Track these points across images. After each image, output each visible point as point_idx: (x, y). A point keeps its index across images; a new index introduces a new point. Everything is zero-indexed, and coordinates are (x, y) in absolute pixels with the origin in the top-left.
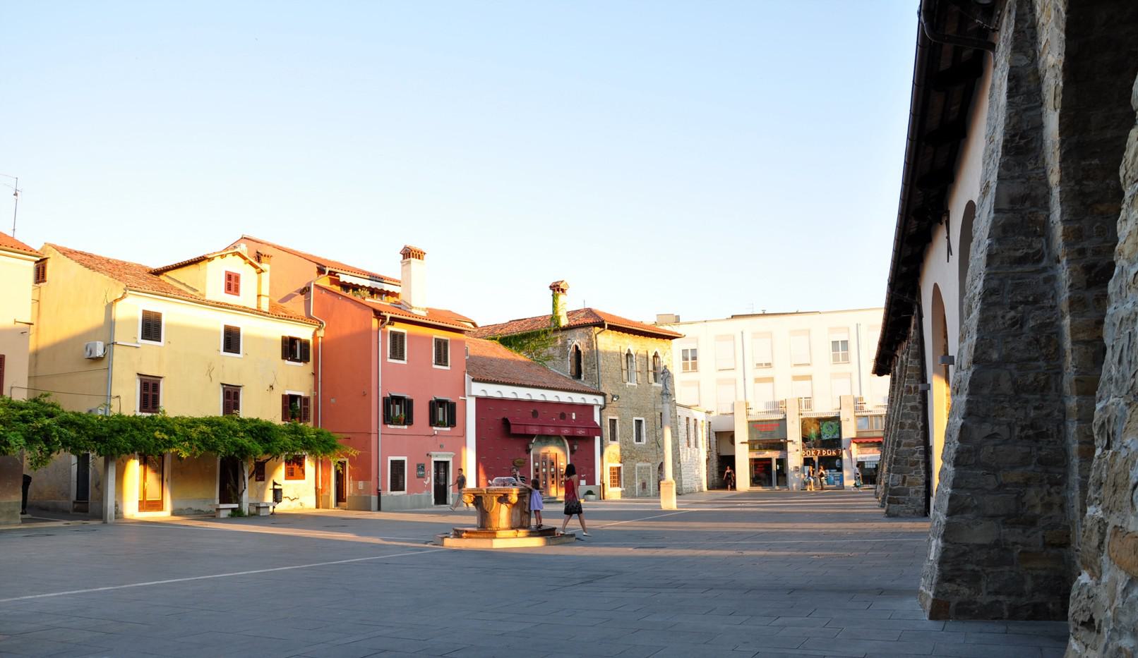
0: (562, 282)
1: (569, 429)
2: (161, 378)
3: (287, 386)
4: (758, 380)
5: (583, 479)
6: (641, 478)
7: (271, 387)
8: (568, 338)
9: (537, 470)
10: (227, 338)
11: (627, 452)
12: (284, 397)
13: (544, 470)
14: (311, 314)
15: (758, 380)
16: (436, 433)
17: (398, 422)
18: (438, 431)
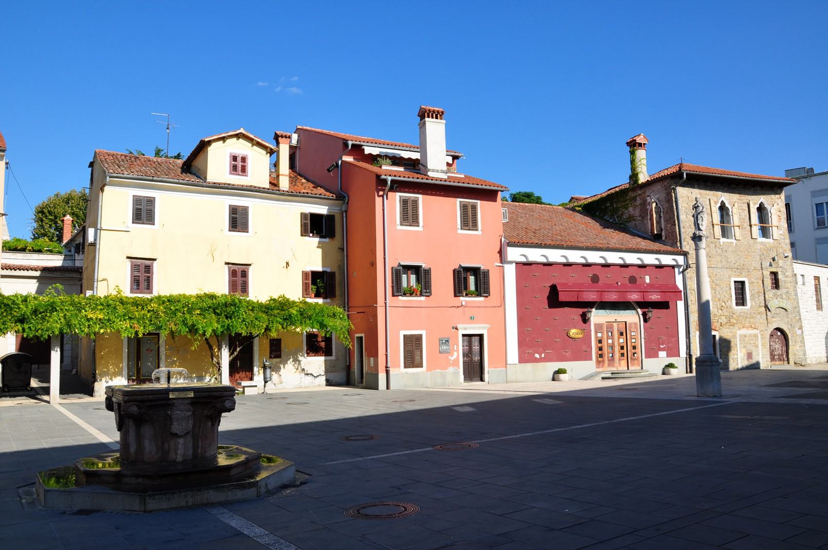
1: (617, 293)
2: (155, 260)
5: (663, 350)
6: (745, 347)
7: (287, 263)
8: (646, 195)
9: (600, 341)
10: (137, 209)
11: (723, 318)
13: (610, 341)
16: (464, 304)
17: (411, 293)
18: (466, 302)
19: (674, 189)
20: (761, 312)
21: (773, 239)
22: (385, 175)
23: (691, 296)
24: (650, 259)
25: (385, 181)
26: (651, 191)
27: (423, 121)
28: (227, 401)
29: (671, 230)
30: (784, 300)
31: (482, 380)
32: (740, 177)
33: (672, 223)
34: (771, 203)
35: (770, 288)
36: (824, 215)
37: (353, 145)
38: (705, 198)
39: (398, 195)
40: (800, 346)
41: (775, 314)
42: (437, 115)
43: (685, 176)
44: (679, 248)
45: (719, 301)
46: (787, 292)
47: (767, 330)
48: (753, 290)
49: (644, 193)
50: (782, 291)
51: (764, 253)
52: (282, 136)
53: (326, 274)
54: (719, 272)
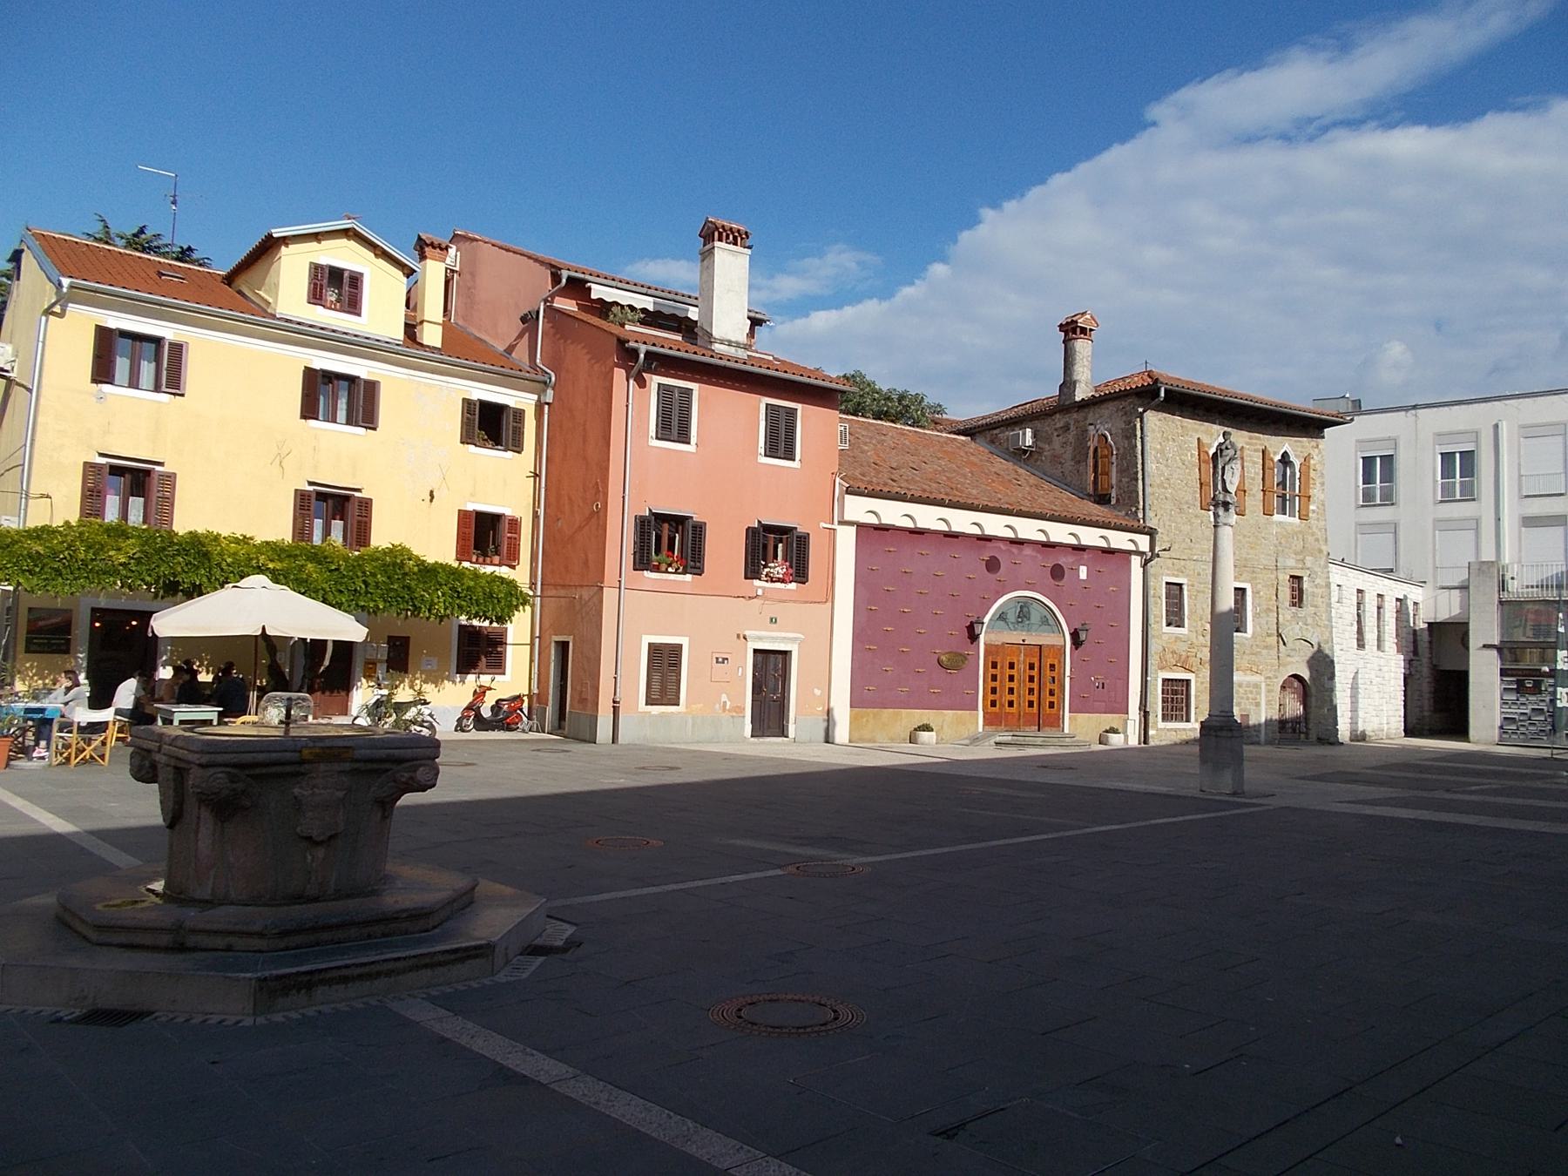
0: (1083, 314)
3: (472, 495)
4: (1529, 522)
12: (463, 516)
14: (538, 361)
15: (1529, 522)
16: (760, 592)
18: (764, 589)
19: (1141, 416)
20: (1271, 645)
21: (1300, 518)
22: (636, 341)
23: (1154, 609)
24: (1091, 537)
25: (634, 353)
26: (1097, 416)
27: (707, 247)
28: (421, 769)
29: (1128, 487)
30: (1309, 627)
31: (783, 732)
32: (1257, 404)
33: (1133, 476)
34: (1301, 454)
35: (1287, 604)
37: (569, 279)
38: (1191, 436)
39: (655, 381)
40: (1328, 710)
41: (1292, 650)
42: (736, 237)
43: (1162, 394)
44: (1142, 521)
45: (1201, 620)
46: (1315, 614)
47: (1276, 678)
48: (1259, 606)
49: (1086, 419)
50: (1307, 610)
51: (1282, 541)
52: (432, 245)
54: (1204, 570)
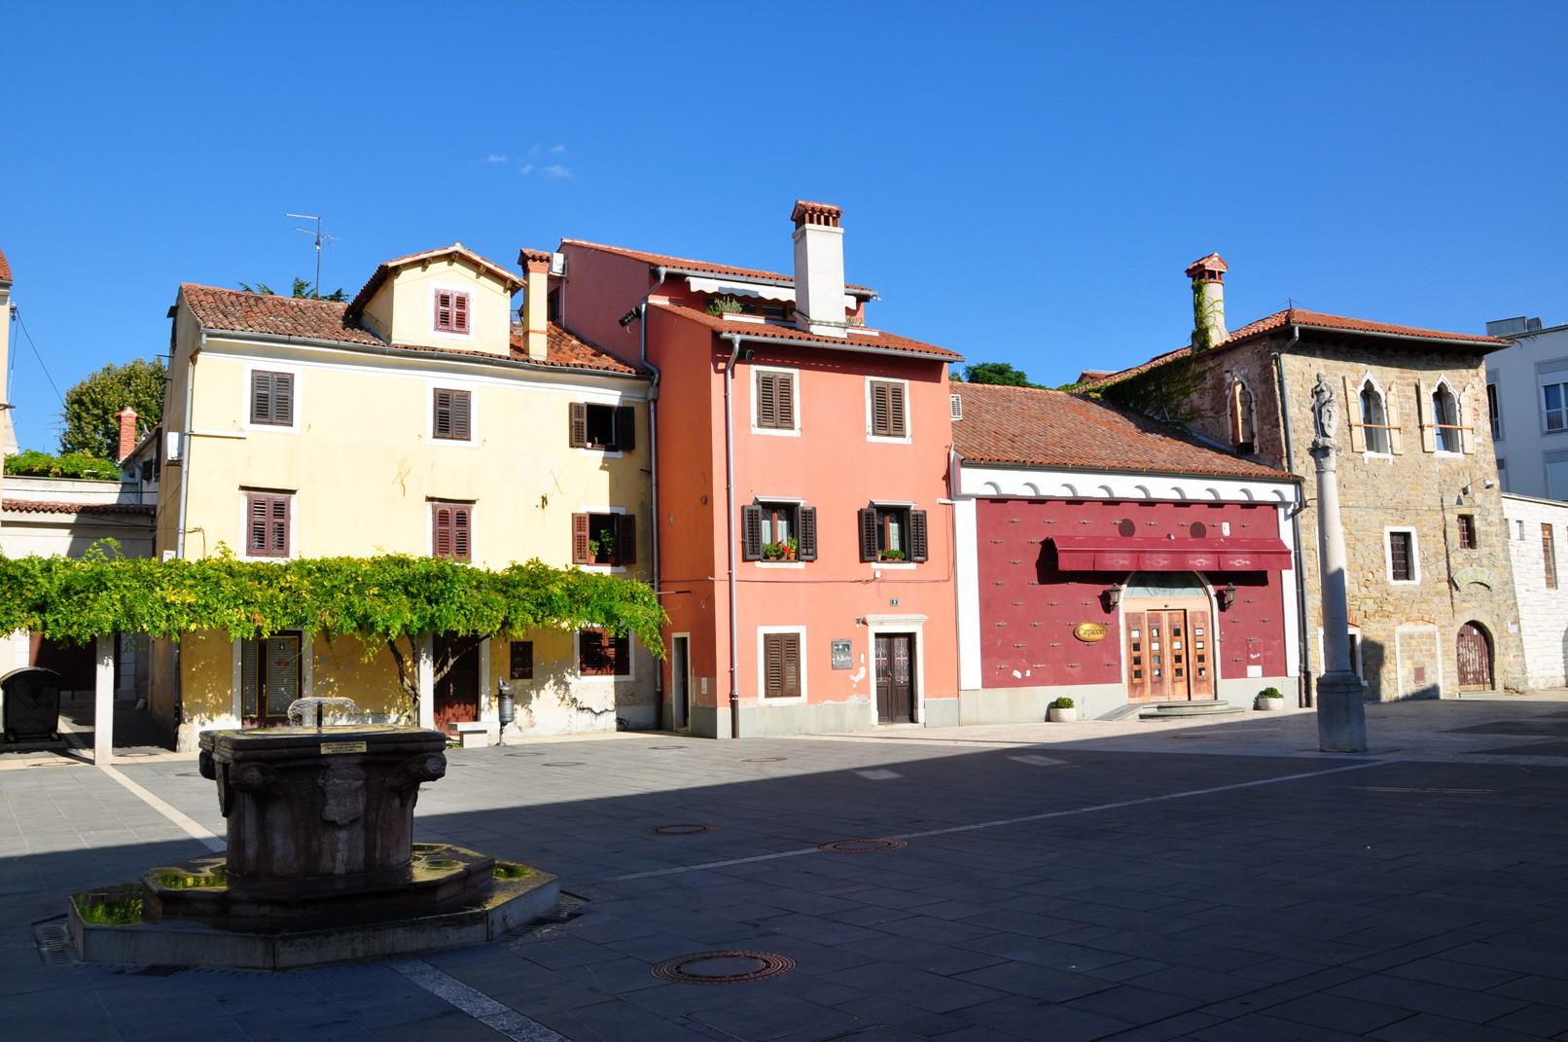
1: (1169, 556)
2: (293, 492)
5: (1255, 662)
6: (1411, 658)
7: (544, 499)
8: (1224, 369)
9: (1136, 647)
10: (260, 396)
11: (1370, 602)
13: (1155, 646)
16: (878, 575)
17: (779, 554)
18: (883, 572)
19: (1277, 359)
20: (1442, 591)
21: (1464, 453)
22: (730, 332)
23: (1308, 562)
24: (1230, 491)
25: (729, 343)
26: (1232, 362)
27: (800, 229)
28: (429, 760)
29: (1270, 435)
30: (1484, 569)
31: (912, 719)
32: (1401, 336)
33: (1273, 423)
34: (1460, 385)
35: (1458, 545)
36: (1560, 407)
37: (668, 275)
38: (1336, 375)
39: (754, 370)
40: (1514, 656)
41: (1467, 595)
42: (828, 218)
43: (1297, 334)
44: (1287, 470)
45: (1362, 570)
46: (1490, 554)
47: (1452, 626)
48: (1426, 549)
49: (1220, 365)
50: (1481, 551)
51: (1447, 479)
52: (534, 259)
53: (618, 520)
54: (1361, 516)
